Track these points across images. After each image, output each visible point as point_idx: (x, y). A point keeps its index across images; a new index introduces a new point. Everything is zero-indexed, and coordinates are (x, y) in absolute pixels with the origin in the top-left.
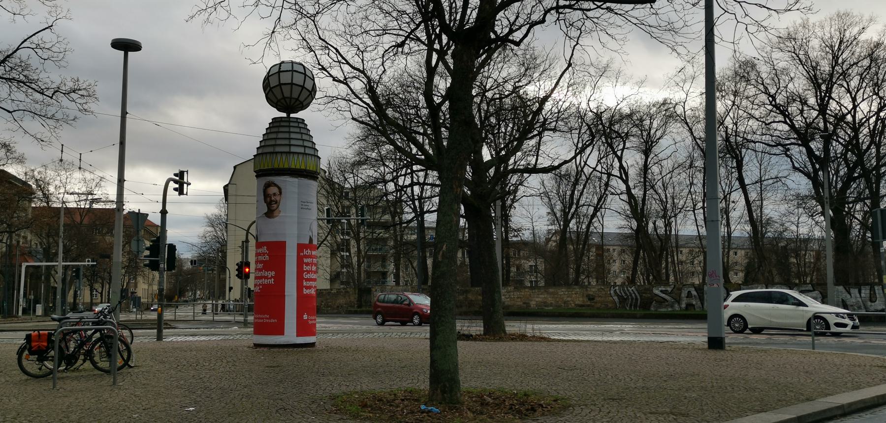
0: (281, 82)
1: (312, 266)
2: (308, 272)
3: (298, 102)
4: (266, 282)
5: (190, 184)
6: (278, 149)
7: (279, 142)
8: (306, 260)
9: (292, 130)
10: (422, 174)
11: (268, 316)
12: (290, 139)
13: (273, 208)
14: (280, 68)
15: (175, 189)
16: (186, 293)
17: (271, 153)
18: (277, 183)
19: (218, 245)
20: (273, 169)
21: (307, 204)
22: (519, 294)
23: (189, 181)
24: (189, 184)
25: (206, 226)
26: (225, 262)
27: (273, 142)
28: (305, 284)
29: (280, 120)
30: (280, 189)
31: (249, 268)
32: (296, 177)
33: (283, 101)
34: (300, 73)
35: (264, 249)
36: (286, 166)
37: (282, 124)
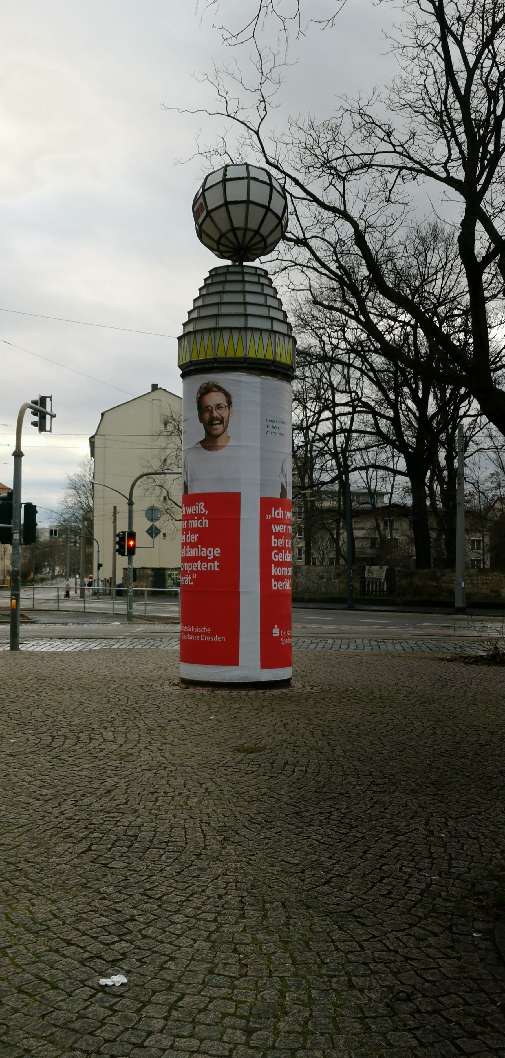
0: (229, 199)
1: (285, 539)
2: (280, 550)
3: (258, 238)
4: (204, 567)
5: (55, 416)
6: (224, 323)
7: (225, 310)
8: (275, 528)
9: (248, 287)
10: (347, 419)
11: (209, 630)
12: (245, 304)
13: (216, 432)
14: (225, 175)
15: (34, 424)
16: (43, 570)
17: (210, 330)
18: (220, 384)
19: (81, 512)
20: (215, 360)
21: (277, 425)
22: (484, 578)
23: (54, 412)
24: (53, 416)
25: (67, 488)
26: (91, 534)
27: (214, 311)
28: (274, 571)
29: (225, 270)
30: (228, 396)
31: (134, 541)
32: (257, 375)
33: (231, 236)
34: (262, 182)
35: (200, 508)
36: (240, 354)
37: (230, 278)
